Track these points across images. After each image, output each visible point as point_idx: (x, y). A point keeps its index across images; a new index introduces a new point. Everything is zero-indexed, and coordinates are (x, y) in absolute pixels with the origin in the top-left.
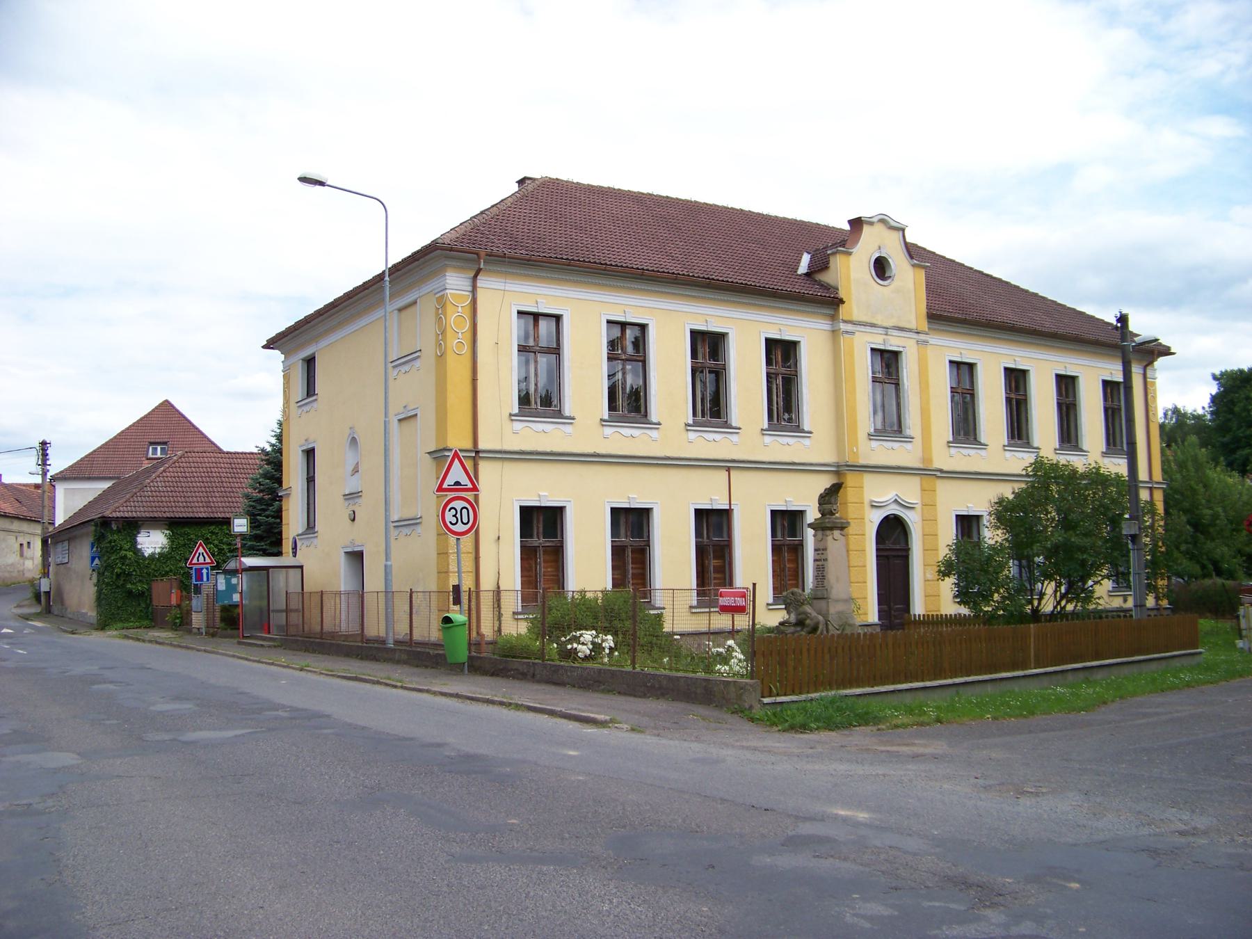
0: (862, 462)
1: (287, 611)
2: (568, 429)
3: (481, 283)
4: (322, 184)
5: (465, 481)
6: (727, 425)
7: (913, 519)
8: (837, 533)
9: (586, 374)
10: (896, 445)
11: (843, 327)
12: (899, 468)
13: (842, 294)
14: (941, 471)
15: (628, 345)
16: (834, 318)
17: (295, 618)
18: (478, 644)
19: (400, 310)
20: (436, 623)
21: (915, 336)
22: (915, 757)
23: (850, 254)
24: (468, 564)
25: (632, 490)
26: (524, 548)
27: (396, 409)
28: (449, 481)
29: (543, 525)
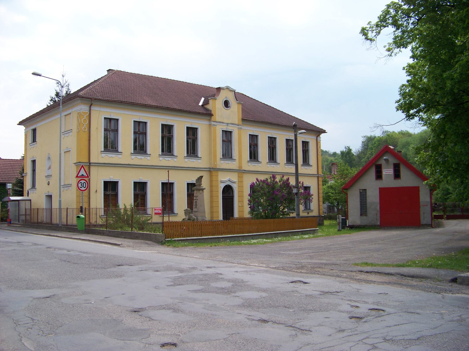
0: (218, 167)
1: (26, 215)
2: (120, 156)
3: (93, 108)
4: (40, 75)
5: (85, 174)
6: (173, 155)
7: (235, 187)
8: (201, 191)
10: (230, 162)
11: (213, 123)
12: (230, 169)
13: (213, 113)
14: (245, 171)
15: (140, 129)
16: (210, 120)
17: (28, 217)
18: (89, 226)
19: (65, 116)
20: (75, 218)
21: (237, 126)
23: (216, 99)
24: (86, 199)
25: (141, 176)
26: (105, 195)
27: (64, 149)
28: (80, 174)
29: (111, 188)
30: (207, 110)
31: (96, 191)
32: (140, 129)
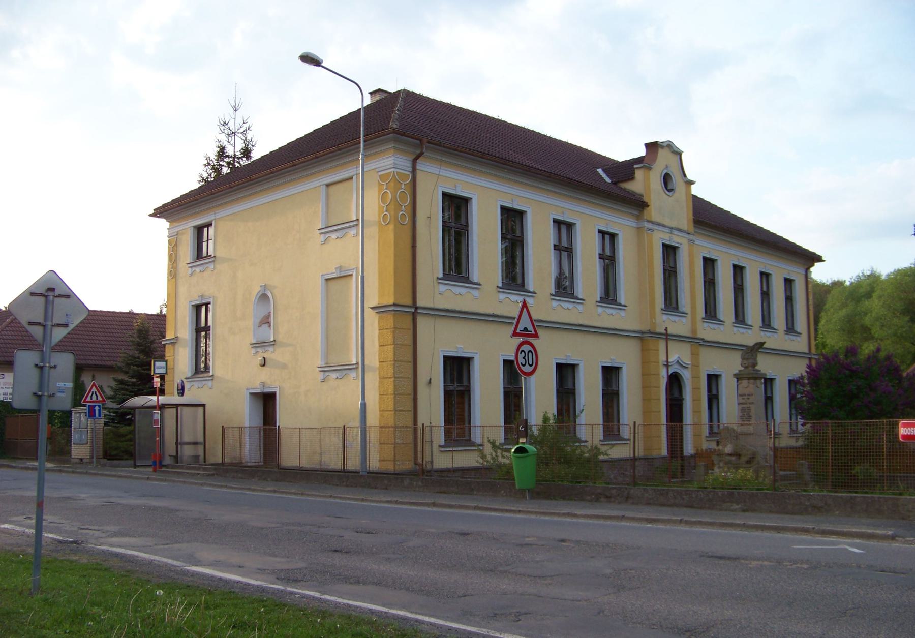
3: (421, 165)
6: (467, 280)
7: (686, 375)
11: (647, 225)
13: (645, 199)
14: (702, 339)
16: (639, 218)
19: (328, 185)
21: (687, 236)
31: (430, 382)
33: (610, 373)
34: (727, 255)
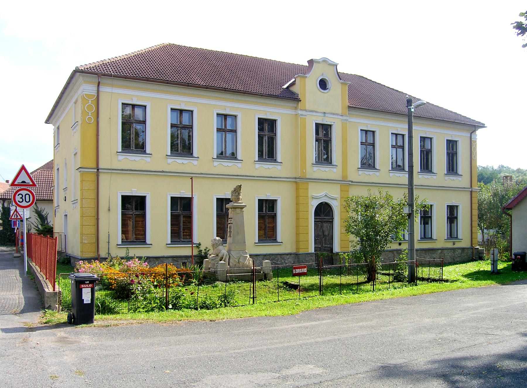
3: (102, 89)
6: (275, 161)
7: (336, 206)
8: (238, 210)
9: (158, 135)
11: (300, 112)
13: (300, 97)
14: (352, 182)
15: (227, 126)
21: (341, 117)
22: (254, 333)
23: (306, 77)
30: (293, 93)
31: (109, 210)
32: (227, 126)
33: (452, 210)
34: (386, 130)
